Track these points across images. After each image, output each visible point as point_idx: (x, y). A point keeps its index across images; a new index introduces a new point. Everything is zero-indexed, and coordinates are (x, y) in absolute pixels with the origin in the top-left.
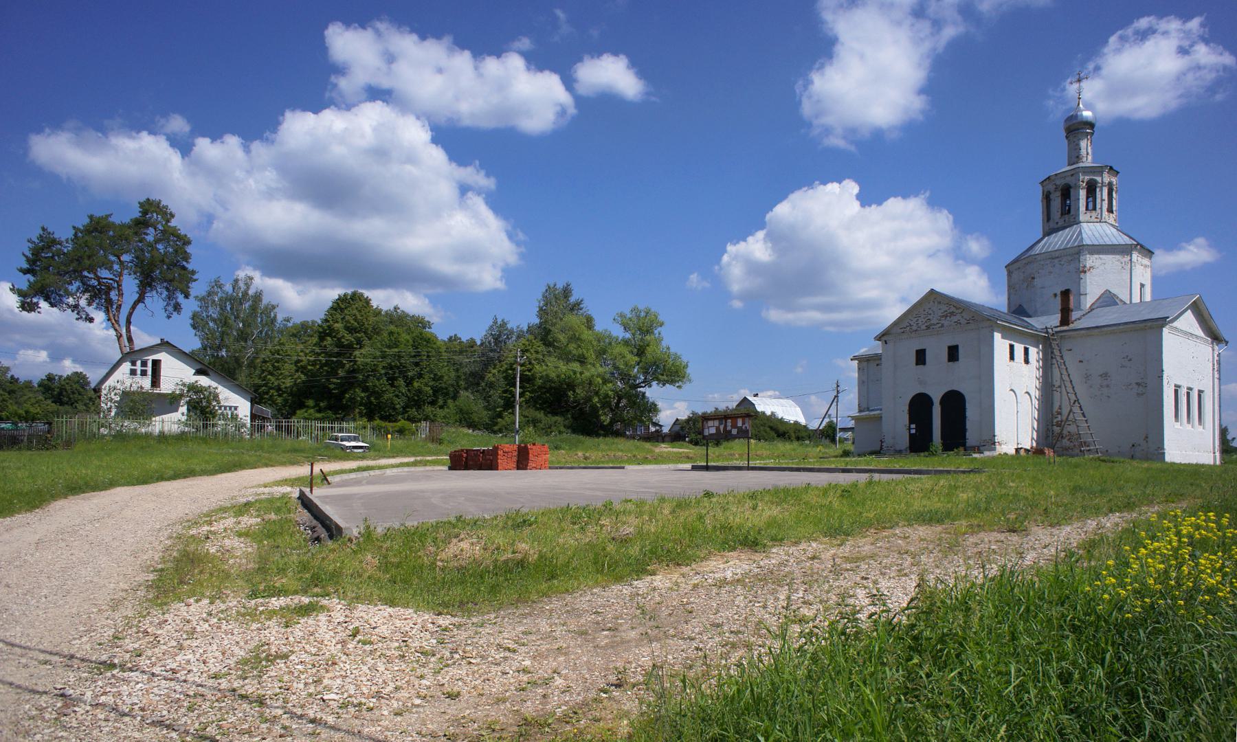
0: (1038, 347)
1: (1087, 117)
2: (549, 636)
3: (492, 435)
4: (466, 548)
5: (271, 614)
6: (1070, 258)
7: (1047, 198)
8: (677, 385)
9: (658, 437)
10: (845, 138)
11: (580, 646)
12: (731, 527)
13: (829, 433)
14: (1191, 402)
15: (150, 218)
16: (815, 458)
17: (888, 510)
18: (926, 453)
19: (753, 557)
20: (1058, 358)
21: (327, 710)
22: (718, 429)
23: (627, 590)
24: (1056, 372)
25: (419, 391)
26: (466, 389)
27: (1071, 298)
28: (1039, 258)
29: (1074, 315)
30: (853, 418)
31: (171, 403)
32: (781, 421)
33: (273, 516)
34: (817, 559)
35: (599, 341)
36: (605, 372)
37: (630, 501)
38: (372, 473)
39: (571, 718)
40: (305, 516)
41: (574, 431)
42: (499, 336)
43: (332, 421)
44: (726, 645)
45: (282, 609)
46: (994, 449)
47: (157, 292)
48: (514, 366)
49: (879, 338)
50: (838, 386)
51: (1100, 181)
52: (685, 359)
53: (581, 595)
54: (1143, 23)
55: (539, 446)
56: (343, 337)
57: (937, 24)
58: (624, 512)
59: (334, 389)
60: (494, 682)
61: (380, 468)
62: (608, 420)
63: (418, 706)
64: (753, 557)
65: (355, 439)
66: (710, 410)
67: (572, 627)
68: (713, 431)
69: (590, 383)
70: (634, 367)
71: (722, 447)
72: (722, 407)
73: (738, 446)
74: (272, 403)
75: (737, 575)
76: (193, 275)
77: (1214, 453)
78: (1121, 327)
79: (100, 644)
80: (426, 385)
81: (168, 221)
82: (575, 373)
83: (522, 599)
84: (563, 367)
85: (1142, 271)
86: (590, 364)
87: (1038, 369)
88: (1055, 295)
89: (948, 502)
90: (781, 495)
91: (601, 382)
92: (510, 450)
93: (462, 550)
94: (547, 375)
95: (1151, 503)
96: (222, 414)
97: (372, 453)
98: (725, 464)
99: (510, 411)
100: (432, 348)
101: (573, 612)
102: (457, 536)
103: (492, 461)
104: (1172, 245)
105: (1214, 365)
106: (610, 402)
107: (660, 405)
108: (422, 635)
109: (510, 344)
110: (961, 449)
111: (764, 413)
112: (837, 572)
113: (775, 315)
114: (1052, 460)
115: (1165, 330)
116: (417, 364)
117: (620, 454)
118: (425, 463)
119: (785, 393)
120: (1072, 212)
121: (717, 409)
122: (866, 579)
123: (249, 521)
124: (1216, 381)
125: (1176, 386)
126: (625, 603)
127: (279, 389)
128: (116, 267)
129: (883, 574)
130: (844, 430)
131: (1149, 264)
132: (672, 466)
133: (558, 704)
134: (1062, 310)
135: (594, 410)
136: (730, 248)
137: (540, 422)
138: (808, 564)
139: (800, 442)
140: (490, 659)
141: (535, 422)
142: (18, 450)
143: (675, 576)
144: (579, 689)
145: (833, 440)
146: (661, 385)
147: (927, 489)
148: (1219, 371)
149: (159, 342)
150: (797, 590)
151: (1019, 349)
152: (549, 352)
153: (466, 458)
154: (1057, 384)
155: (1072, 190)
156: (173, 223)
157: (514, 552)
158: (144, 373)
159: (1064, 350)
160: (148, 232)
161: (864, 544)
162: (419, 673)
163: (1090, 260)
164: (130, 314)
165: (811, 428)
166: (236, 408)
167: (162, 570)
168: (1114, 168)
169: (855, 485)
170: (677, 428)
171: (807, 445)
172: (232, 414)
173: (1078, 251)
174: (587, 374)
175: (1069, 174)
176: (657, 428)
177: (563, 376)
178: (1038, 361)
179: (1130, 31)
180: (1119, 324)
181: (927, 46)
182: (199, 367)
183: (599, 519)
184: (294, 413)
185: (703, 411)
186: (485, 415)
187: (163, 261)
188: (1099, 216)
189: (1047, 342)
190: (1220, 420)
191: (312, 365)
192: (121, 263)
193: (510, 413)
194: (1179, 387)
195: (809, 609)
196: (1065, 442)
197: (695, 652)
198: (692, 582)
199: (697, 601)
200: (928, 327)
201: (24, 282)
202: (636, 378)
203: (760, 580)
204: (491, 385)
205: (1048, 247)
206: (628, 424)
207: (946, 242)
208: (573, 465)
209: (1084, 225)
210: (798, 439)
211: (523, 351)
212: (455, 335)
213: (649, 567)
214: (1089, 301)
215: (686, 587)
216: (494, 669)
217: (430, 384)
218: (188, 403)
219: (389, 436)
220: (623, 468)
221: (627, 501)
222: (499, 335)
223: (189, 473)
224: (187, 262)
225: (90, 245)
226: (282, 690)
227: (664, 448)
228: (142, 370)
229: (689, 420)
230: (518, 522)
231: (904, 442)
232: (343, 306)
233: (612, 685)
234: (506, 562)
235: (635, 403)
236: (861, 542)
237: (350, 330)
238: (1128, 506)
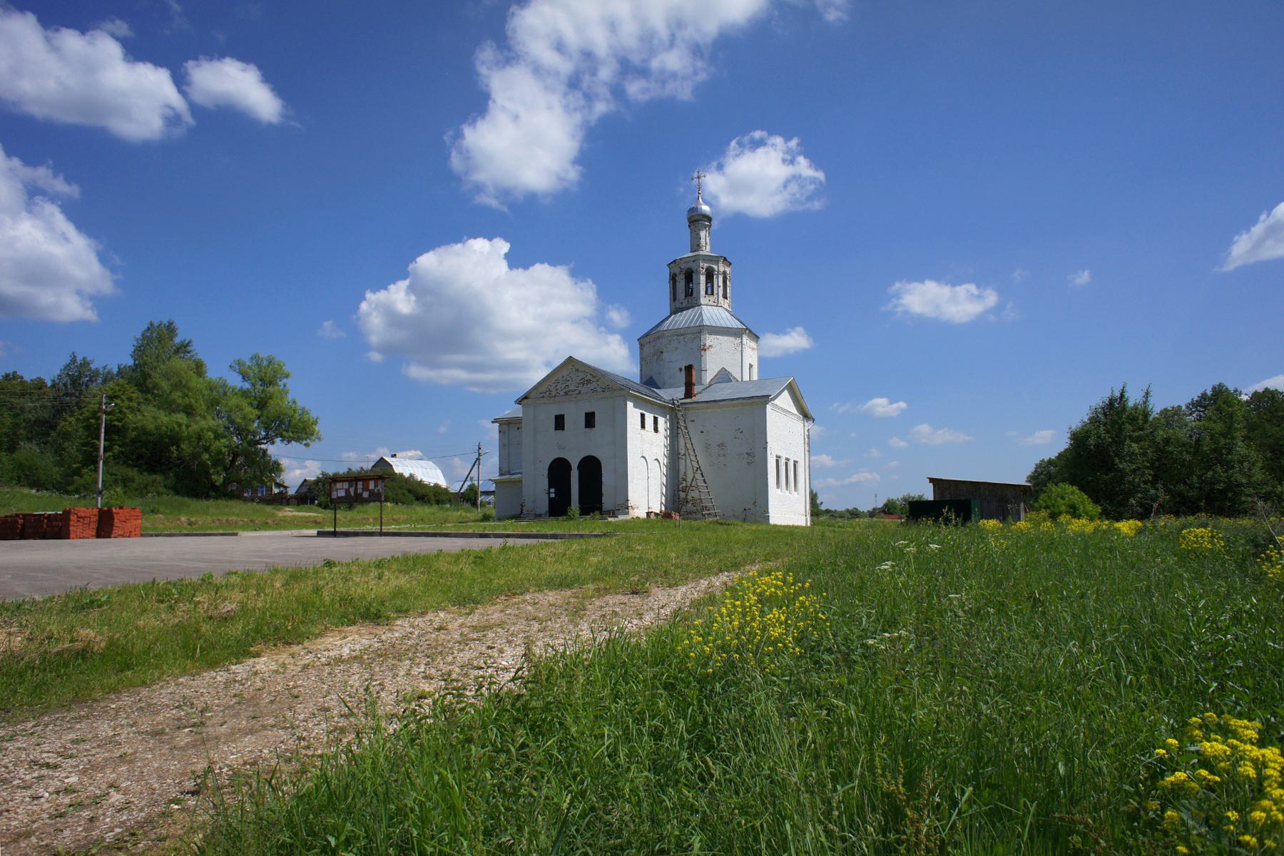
0: (665, 417)
2: (112, 741)
3: (65, 496)
7: (673, 278)
8: (305, 442)
9: (282, 499)
10: (497, 197)
11: (151, 750)
12: (352, 599)
13: (470, 497)
14: (788, 470)
16: (454, 522)
18: (565, 517)
19: (374, 631)
20: (683, 428)
22: (347, 491)
23: (221, 676)
26: (29, 440)
27: (694, 373)
29: (697, 389)
30: (496, 482)
32: (420, 483)
34: (443, 629)
35: (211, 390)
36: (218, 426)
37: (236, 573)
39: (126, 841)
41: (177, 492)
44: (334, 731)
46: (628, 513)
48: (99, 414)
49: (519, 402)
50: (480, 448)
52: (313, 415)
54: (757, 134)
55: (127, 508)
57: (589, 98)
58: (226, 585)
60: (16, 813)
62: (221, 480)
64: (374, 631)
66: (342, 470)
67: (144, 727)
68: (342, 494)
69: (199, 438)
70: (253, 421)
71: (357, 509)
72: (356, 467)
73: (372, 509)
75: (354, 651)
78: (734, 402)
82: (180, 425)
83: (78, 699)
84: (164, 418)
85: (751, 353)
86: (200, 415)
88: (681, 370)
90: (409, 563)
91: (212, 437)
92: (88, 515)
95: (753, 562)
98: (357, 529)
99: (92, 467)
101: (151, 709)
104: (780, 330)
106: (224, 459)
107: (284, 462)
109: (94, 388)
110: (597, 512)
111: (401, 475)
112: (464, 641)
113: (416, 372)
115: (769, 407)
117: (234, 518)
119: (429, 454)
121: (350, 469)
122: (492, 648)
125: (777, 456)
126: (218, 692)
129: (509, 642)
130: (487, 493)
131: (755, 347)
132: (295, 532)
133: (109, 826)
136: (369, 295)
137: (133, 481)
138: (433, 636)
139: (440, 506)
141: (125, 482)
143: (284, 657)
144: (144, 803)
145: (474, 504)
146: (285, 442)
147: (559, 554)
148: (809, 444)
150: (419, 664)
151: (649, 418)
152: (146, 399)
153: (23, 525)
154: (682, 452)
155: (694, 276)
157: (72, 641)
159: (688, 420)
161: (493, 613)
163: (709, 340)
169: (488, 551)
170: (305, 490)
171: (447, 510)
174: (195, 427)
176: (282, 489)
177: (164, 428)
178: (666, 430)
179: (746, 139)
180: (733, 400)
181: (578, 118)
183: (194, 596)
185: (335, 471)
186: (56, 473)
189: (673, 412)
193: (91, 470)
195: (430, 684)
197: (297, 742)
198: (302, 663)
199: (307, 683)
202: (254, 434)
203: (380, 656)
204: (66, 436)
205: (674, 325)
206: (244, 485)
207: (586, 310)
208: (173, 531)
210: (438, 502)
211: (111, 398)
213: (252, 649)
214: (708, 376)
215: (293, 669)
216: (19, 795)
220: (236, 534)
221: (230, 574)
227: (289, 512)
229: (318, 481)
231: (544, 506)
233: (188, 793)
235: (254, 462)
236: (490, 609)
238: (735, 566)
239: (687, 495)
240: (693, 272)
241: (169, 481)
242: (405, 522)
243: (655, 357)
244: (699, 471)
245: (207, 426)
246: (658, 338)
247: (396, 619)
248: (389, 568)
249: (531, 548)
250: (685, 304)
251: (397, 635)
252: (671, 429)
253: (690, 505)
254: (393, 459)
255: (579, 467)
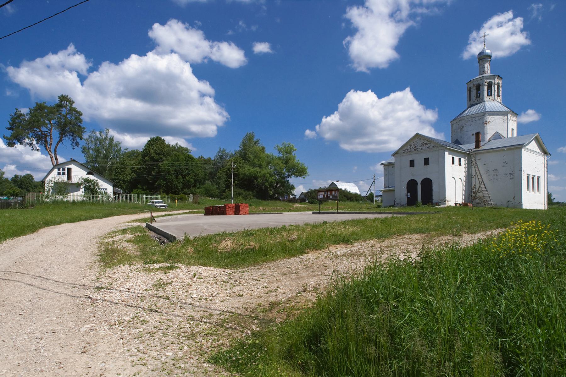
0: (465, 158)
1: (488, 53)
4: (228, 244)
5: (157, 269)
6: (480, 118)
7: (470, 90)
8: (303, 177)
9: (294, 200)
11: (285, 279)
13: (370, 198)
14: (534, 182)
15: (64, 104)
17: (401, 228)
19: (347, 247)
20: (474, 163)
21: (195, 301)
22: (324, 196)
23: (298, 259)
24: (473, 169)
25: (188, 181)
27: (480, 136)
28: (466, 118)
29: (482, 143)
30: (384, 191)
31: (77, 187)
32: (349, 193)
33: (139, 234)
37: (293, 225)
38: (172, 217)
40: (152, 234)
42: (222, 156)
43: (150, 195)
45: (160, 268)
46: (445, 204)
47: (68, 137)
48: (230, 169)
49: (393, 155)
51: (494, 82)
52: (306, 166)
53: (279, 262)
56: (154, 156)
59: (150, 180)
61: (175, 215)
63: (228, 299)
64: (347, 247)
65: (161, 202)
68: (322, 197)
69: (264, 177)
71: (324, 204)
72: (323, 187)
74: (121, 187)
76: (84, 129)
77: (545, 204)
79: (93, 281)
80: (192, 178)
81: (72, 105)
82: (257, 172)
84: (252, 170)
87: (465, 168)
88: (473, 135)
89: (427, 225)
90: (358, 222)
92: (232, 206)
93: (227, 245)
94: (245, 173)
96: (100, 192)
97: (169, 209)
100: (194, 162)
102: (224, 239)
103: (223, 211)
105: (544, 165)
106: (273, 185)
108: (221, 276)
111: (341, 189)
114: (471, 208)
115: (523, 150)
116: (187, 169)
118: (194, 213)
120: (481, 97)
123: (128, 236)
124: (546, 172)
125: (527, 175)
127: (124, 181)
128: (49, 126)
130: (377, 196)
131: (515, 120)
134: (476, 142)
135: (266, 188)
137: (242, 194)
139: (358, 202)
140: (251, 284)
142: (10, 209)
143: (317, 254)
144: (289, 293)
145: (372, 201)
148: (547, 168)
149: (70, 160)
153: (212, 210)
154: (474, 175)
155: (481, 87)
156: (74, 106)
158: (64, 174)
160: (63, 110)
162: (225, 288)
163: (489, 118)
164: (56, 147)
165: (362, 196)
166: (106, 189)
167: (101, 255)
168: (500, 76)
169: (386, 218)
170: (303, 196)
171: (361, 204)
172: (104, 192)
173: (484, 114)
174: (263, 172)
175: (480, 79)
177: (252, 174)
178: (465, 164)
182: (89, 171)
184: (132, 191)
187: (70, 123)
188: (493, 98)
189: (469, 155)
190: (547, 190)
191: (139, 170)
192: (51, 124)
193: (228, 190)
194: (529, 175)
196: (477, 200)
199: (328, 262)
200: (415, 150)
201: (9, 133)
202: (284, 174)
204: (220, 178)
206: (282, 194)
209: (486, 102)
210: (357, 200)
212: (201, 156)
214: (488, 137)
217: (193, 178)
218: (84, 187)
219: (176, 201)
220: (282, 213)
221: (291, 225)
222: (222, 156)
223: (91, 218)
224: (81, 123)
225: (37, 116)
226: (174, 294)
227: (297, 205)
228: (63, 173)
230: (247, 234)
231: (405, 201)
232: (152, 143)
234: (247, 249)
236: (391, 240)
237: (157, 154)
238: (505, 226)
239: (476, 195)
240: (480, 85)
241: (254, 194)
242: (344, 209)
243: (459, 130)
244: (482, 183)
245: (266, 172)
246: (461, 120)
247: (355, 242)
248: (348, 224)
249: (404, 218)
250: (476, 102)
251: (356, 248)
252: (468, 164)
253: (477, 200)
254: (337, 183)
255: (421, 184)
